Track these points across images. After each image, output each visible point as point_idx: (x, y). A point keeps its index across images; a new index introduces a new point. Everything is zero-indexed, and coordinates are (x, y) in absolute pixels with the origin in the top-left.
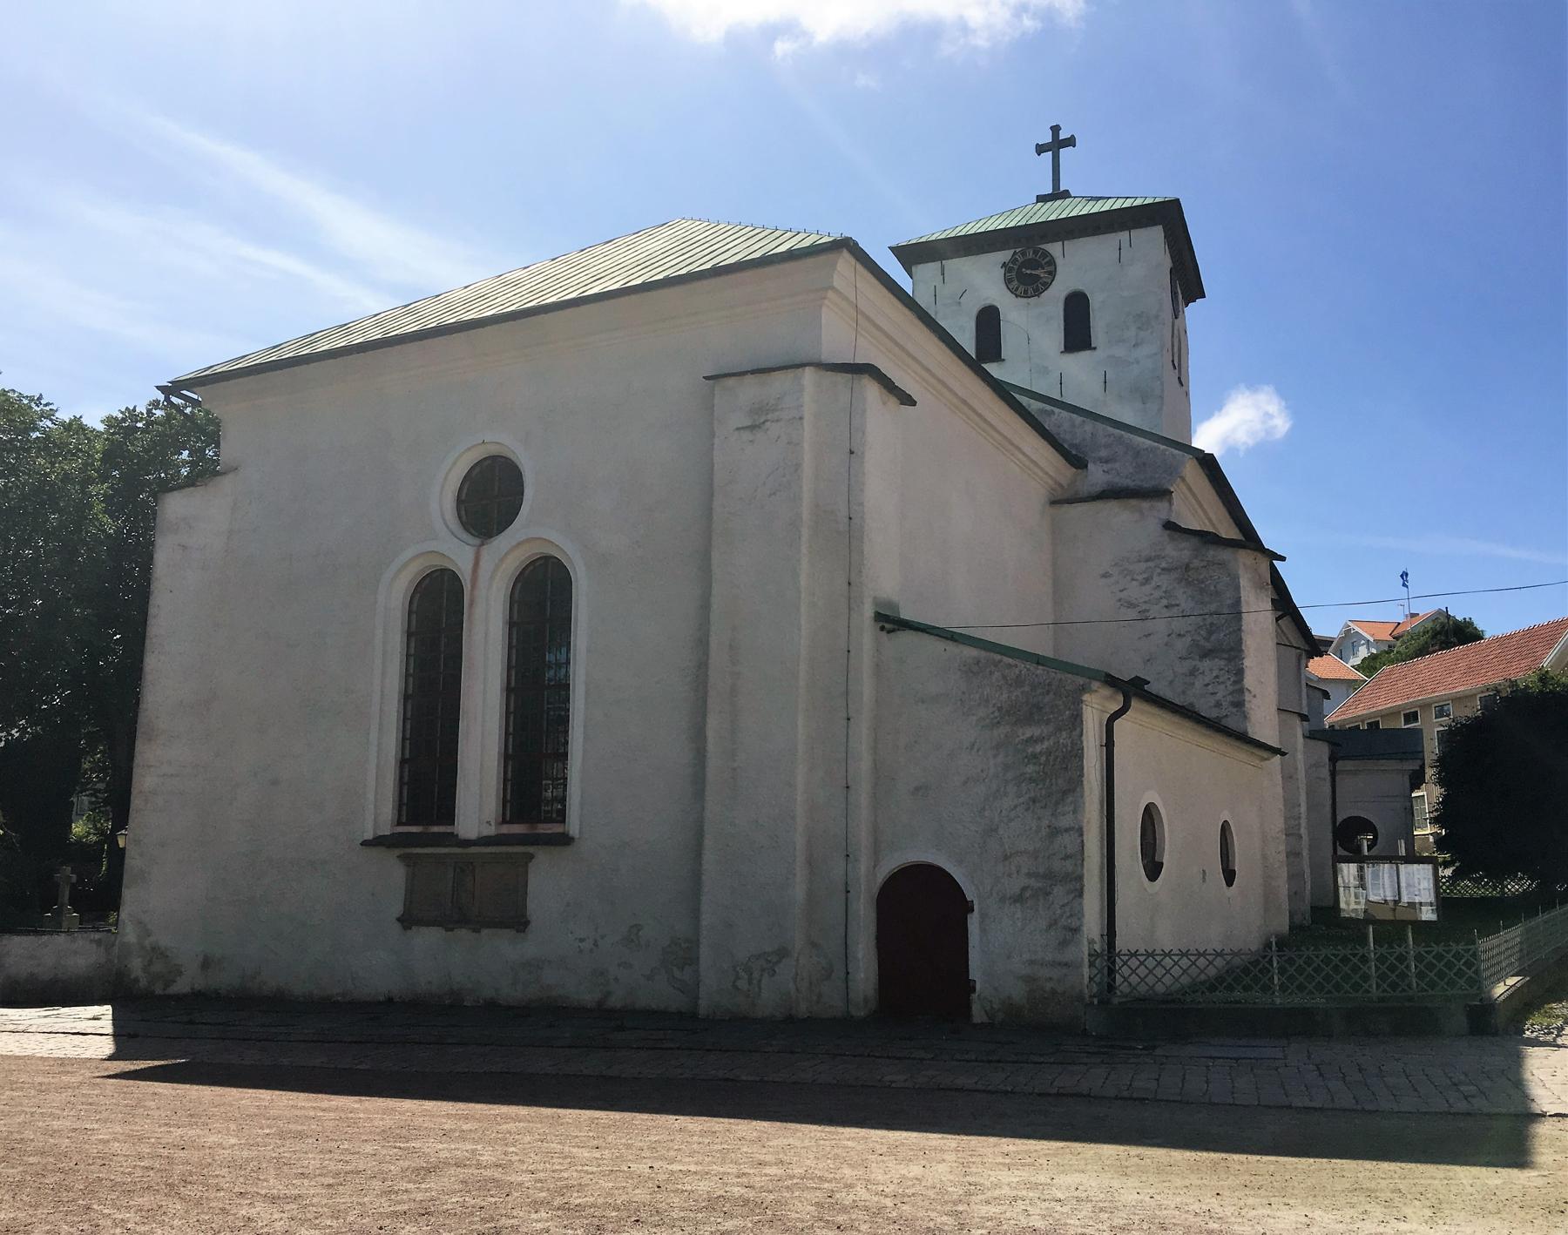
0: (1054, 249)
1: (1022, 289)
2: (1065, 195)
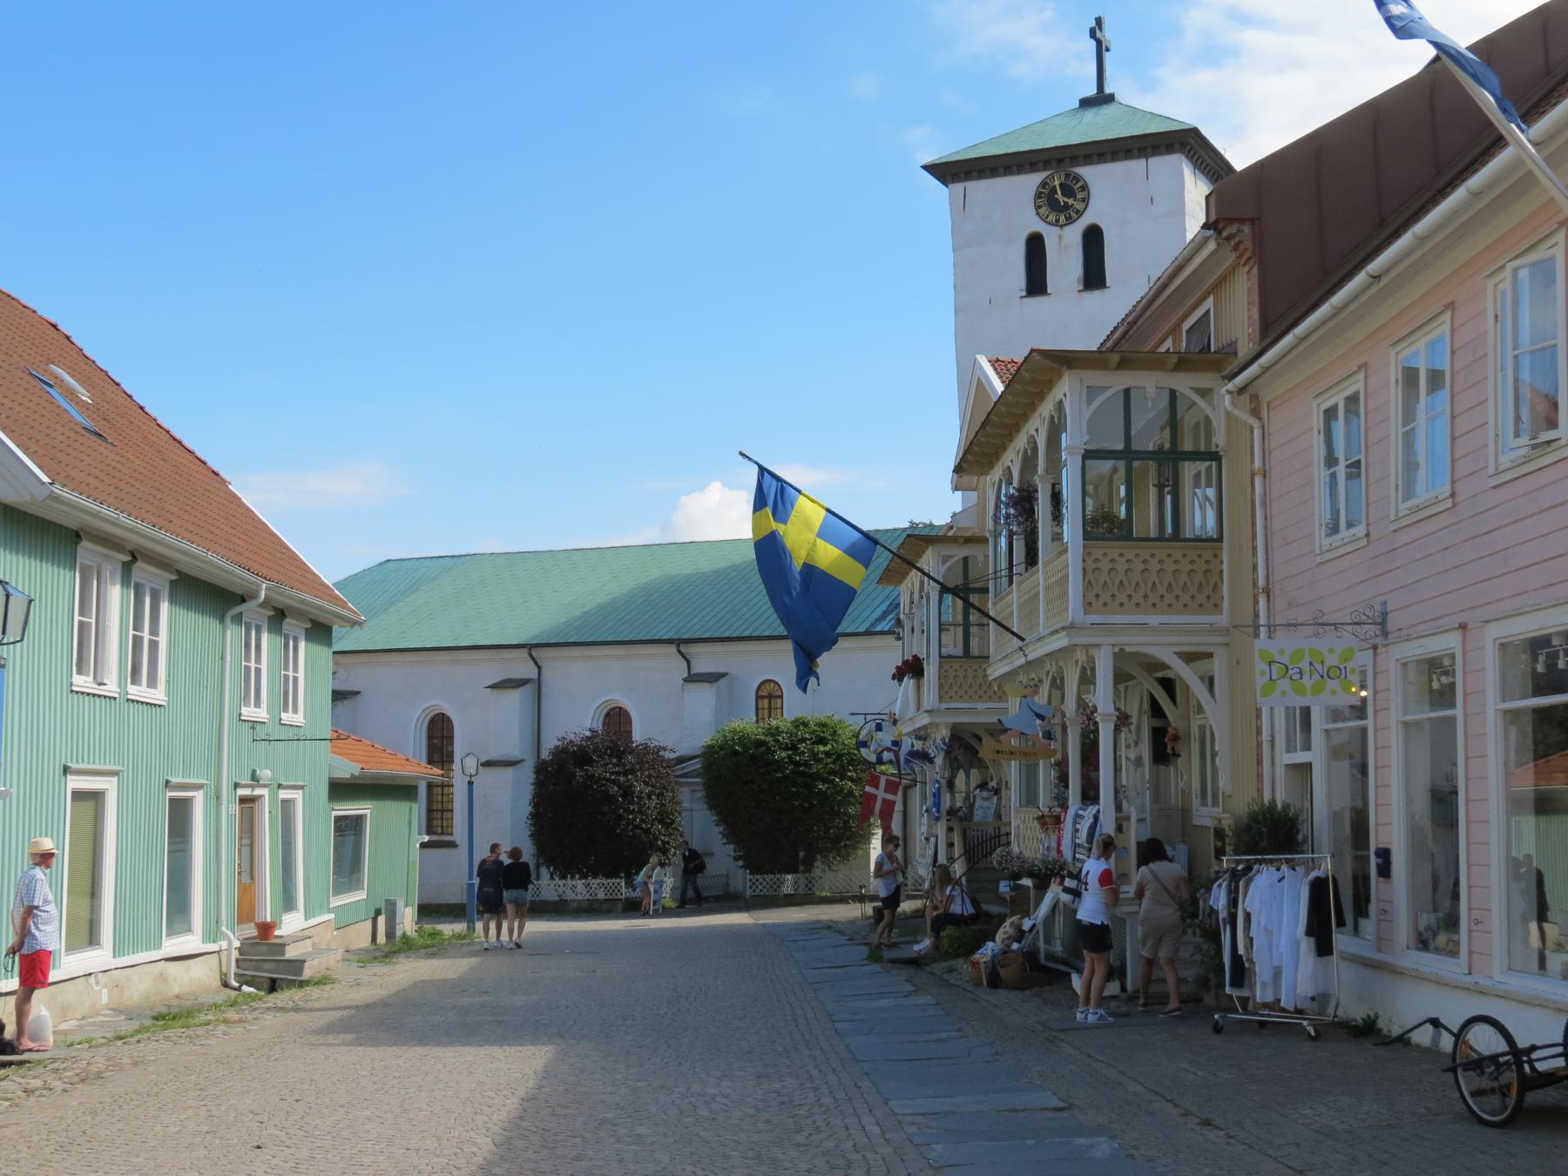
0: (1088, 173)
1: (1062, 219)
2: (1110, 99)
